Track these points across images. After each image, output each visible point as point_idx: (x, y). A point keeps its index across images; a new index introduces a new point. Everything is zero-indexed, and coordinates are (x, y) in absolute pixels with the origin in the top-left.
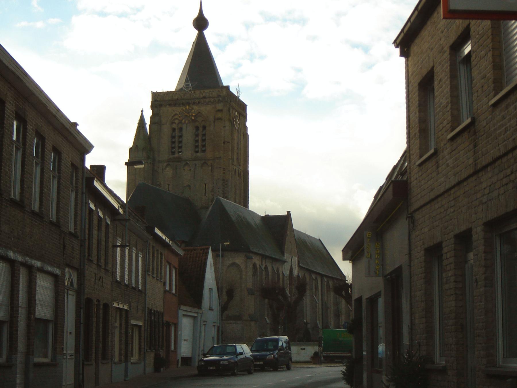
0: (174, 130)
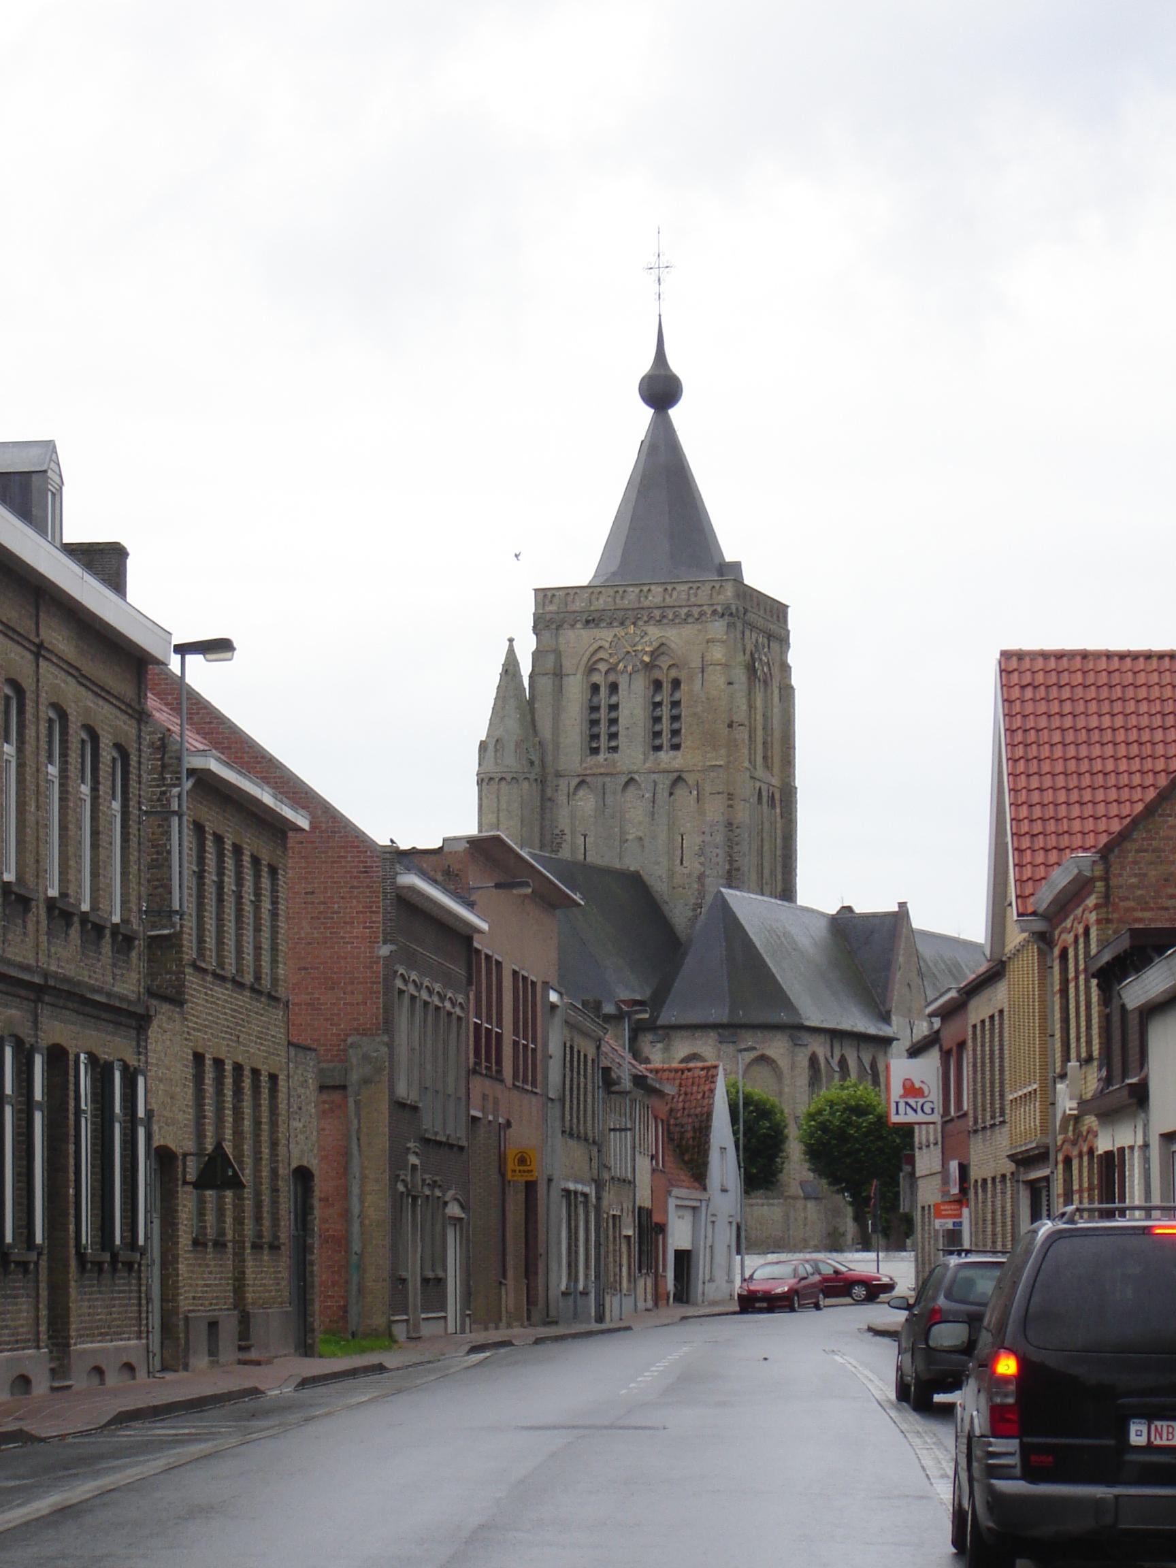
0: (595, 688)
